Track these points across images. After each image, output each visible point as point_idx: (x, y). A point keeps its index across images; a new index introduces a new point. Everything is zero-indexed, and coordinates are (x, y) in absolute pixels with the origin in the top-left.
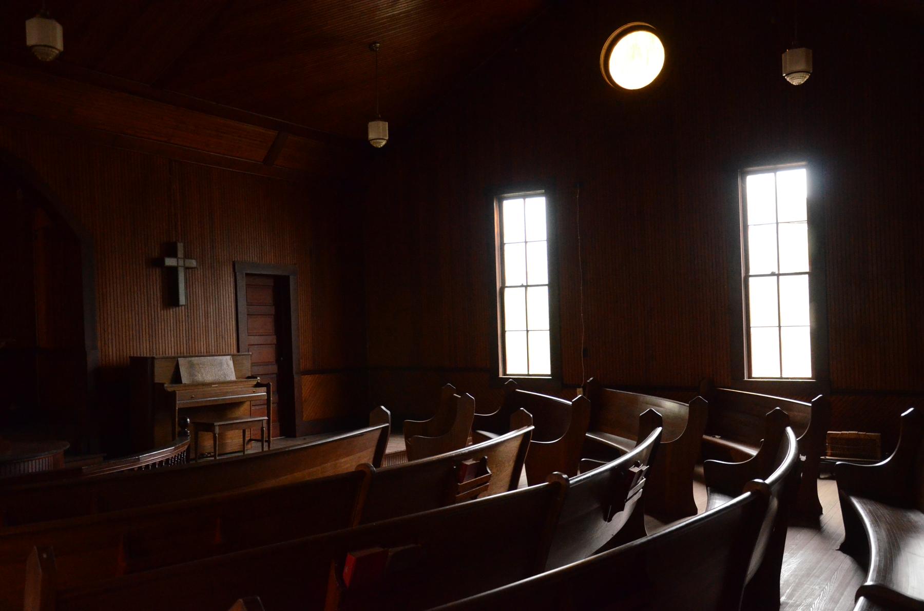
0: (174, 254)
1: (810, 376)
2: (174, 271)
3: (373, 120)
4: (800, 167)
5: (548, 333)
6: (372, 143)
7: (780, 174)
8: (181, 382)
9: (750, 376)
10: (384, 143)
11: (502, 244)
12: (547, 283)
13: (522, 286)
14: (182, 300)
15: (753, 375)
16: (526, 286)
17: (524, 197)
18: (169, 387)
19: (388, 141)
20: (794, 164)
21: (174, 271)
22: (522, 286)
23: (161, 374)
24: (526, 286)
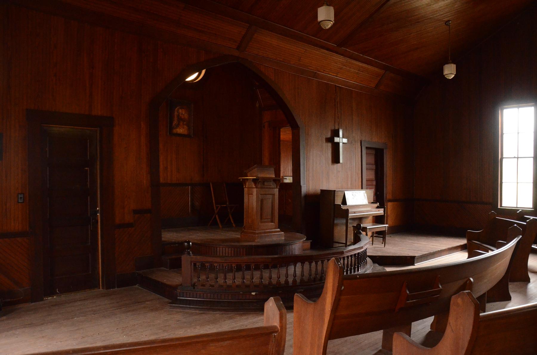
0: (338, 136)
1: (531, 207)
2: (338, 144)
3: (448, 64)
4: (531, 106)
5: (532, 184)
6: (446, 76)
7: (521, 109)
8: (346, 204)
9: (501, 206)
10: (453, 76)
11: (502, 134)
12: (533, 156)
13: (515, 157)
14: (341, 161)
15: (503, 205)
16: (518, 158)
17: (518, 107)
18: (343, 207)
19: (455, 75)
20: (521, 105)
21: (338, 144)
22: (515, 157)
23: (338, 201)
24: (518, 158)
